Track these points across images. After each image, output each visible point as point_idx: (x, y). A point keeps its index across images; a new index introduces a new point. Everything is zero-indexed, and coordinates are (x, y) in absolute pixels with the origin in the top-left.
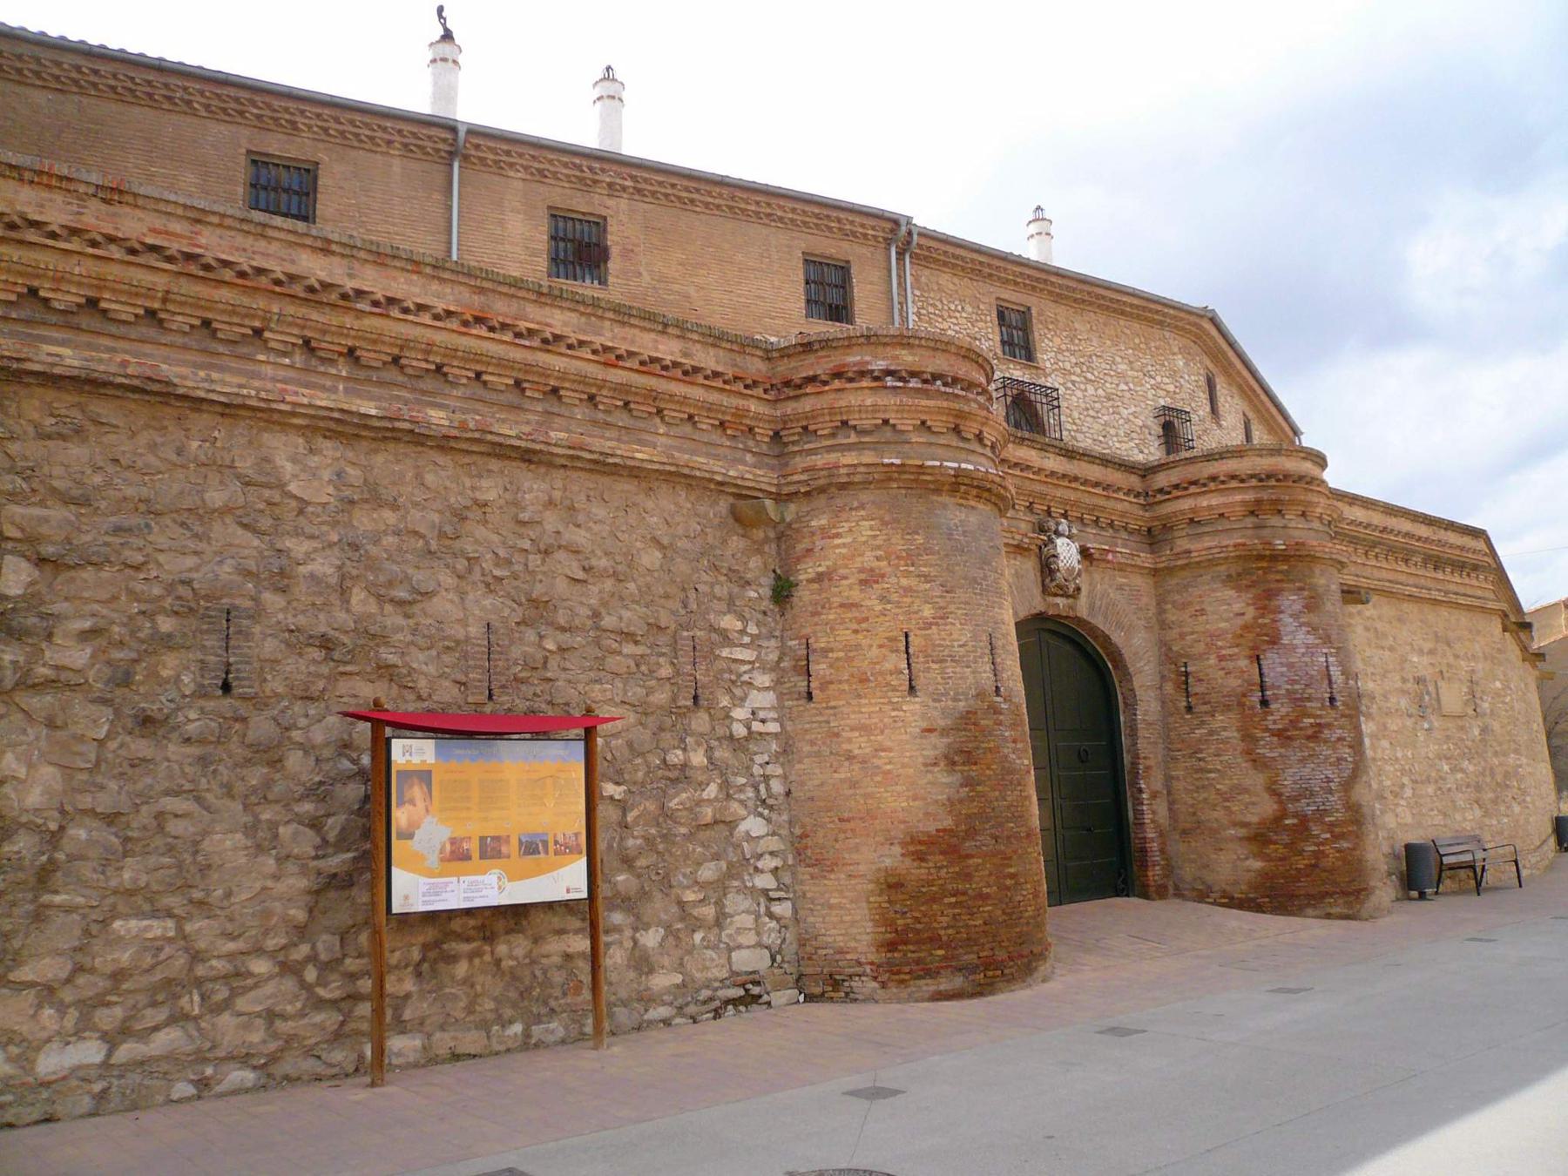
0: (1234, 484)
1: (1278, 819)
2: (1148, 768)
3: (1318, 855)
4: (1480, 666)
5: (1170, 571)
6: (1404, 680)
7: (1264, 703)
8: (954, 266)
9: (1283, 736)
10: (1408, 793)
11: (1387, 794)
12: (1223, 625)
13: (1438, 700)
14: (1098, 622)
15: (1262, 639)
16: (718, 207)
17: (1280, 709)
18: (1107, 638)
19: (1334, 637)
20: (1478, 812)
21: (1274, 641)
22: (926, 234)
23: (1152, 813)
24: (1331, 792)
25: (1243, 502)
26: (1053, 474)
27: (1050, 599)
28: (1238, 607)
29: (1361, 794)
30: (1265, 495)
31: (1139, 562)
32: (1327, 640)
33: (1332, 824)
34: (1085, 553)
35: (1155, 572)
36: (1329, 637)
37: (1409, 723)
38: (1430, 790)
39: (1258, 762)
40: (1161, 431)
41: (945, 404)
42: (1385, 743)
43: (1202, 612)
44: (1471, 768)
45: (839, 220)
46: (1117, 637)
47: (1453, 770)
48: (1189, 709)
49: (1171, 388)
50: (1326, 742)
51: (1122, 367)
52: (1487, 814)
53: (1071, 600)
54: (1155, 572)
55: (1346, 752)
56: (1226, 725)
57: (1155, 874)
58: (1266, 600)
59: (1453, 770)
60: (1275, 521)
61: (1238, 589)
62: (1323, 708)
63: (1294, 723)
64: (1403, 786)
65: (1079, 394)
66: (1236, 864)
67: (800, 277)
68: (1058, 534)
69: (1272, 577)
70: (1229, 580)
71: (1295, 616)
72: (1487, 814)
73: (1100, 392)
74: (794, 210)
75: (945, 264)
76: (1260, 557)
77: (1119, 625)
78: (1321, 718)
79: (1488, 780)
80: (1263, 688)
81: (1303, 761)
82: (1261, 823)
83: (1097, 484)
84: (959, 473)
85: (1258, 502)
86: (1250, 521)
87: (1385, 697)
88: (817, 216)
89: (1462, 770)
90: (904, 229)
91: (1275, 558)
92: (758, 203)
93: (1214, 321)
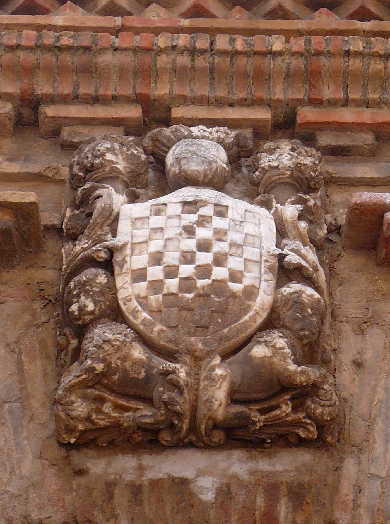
68: (155, 178)
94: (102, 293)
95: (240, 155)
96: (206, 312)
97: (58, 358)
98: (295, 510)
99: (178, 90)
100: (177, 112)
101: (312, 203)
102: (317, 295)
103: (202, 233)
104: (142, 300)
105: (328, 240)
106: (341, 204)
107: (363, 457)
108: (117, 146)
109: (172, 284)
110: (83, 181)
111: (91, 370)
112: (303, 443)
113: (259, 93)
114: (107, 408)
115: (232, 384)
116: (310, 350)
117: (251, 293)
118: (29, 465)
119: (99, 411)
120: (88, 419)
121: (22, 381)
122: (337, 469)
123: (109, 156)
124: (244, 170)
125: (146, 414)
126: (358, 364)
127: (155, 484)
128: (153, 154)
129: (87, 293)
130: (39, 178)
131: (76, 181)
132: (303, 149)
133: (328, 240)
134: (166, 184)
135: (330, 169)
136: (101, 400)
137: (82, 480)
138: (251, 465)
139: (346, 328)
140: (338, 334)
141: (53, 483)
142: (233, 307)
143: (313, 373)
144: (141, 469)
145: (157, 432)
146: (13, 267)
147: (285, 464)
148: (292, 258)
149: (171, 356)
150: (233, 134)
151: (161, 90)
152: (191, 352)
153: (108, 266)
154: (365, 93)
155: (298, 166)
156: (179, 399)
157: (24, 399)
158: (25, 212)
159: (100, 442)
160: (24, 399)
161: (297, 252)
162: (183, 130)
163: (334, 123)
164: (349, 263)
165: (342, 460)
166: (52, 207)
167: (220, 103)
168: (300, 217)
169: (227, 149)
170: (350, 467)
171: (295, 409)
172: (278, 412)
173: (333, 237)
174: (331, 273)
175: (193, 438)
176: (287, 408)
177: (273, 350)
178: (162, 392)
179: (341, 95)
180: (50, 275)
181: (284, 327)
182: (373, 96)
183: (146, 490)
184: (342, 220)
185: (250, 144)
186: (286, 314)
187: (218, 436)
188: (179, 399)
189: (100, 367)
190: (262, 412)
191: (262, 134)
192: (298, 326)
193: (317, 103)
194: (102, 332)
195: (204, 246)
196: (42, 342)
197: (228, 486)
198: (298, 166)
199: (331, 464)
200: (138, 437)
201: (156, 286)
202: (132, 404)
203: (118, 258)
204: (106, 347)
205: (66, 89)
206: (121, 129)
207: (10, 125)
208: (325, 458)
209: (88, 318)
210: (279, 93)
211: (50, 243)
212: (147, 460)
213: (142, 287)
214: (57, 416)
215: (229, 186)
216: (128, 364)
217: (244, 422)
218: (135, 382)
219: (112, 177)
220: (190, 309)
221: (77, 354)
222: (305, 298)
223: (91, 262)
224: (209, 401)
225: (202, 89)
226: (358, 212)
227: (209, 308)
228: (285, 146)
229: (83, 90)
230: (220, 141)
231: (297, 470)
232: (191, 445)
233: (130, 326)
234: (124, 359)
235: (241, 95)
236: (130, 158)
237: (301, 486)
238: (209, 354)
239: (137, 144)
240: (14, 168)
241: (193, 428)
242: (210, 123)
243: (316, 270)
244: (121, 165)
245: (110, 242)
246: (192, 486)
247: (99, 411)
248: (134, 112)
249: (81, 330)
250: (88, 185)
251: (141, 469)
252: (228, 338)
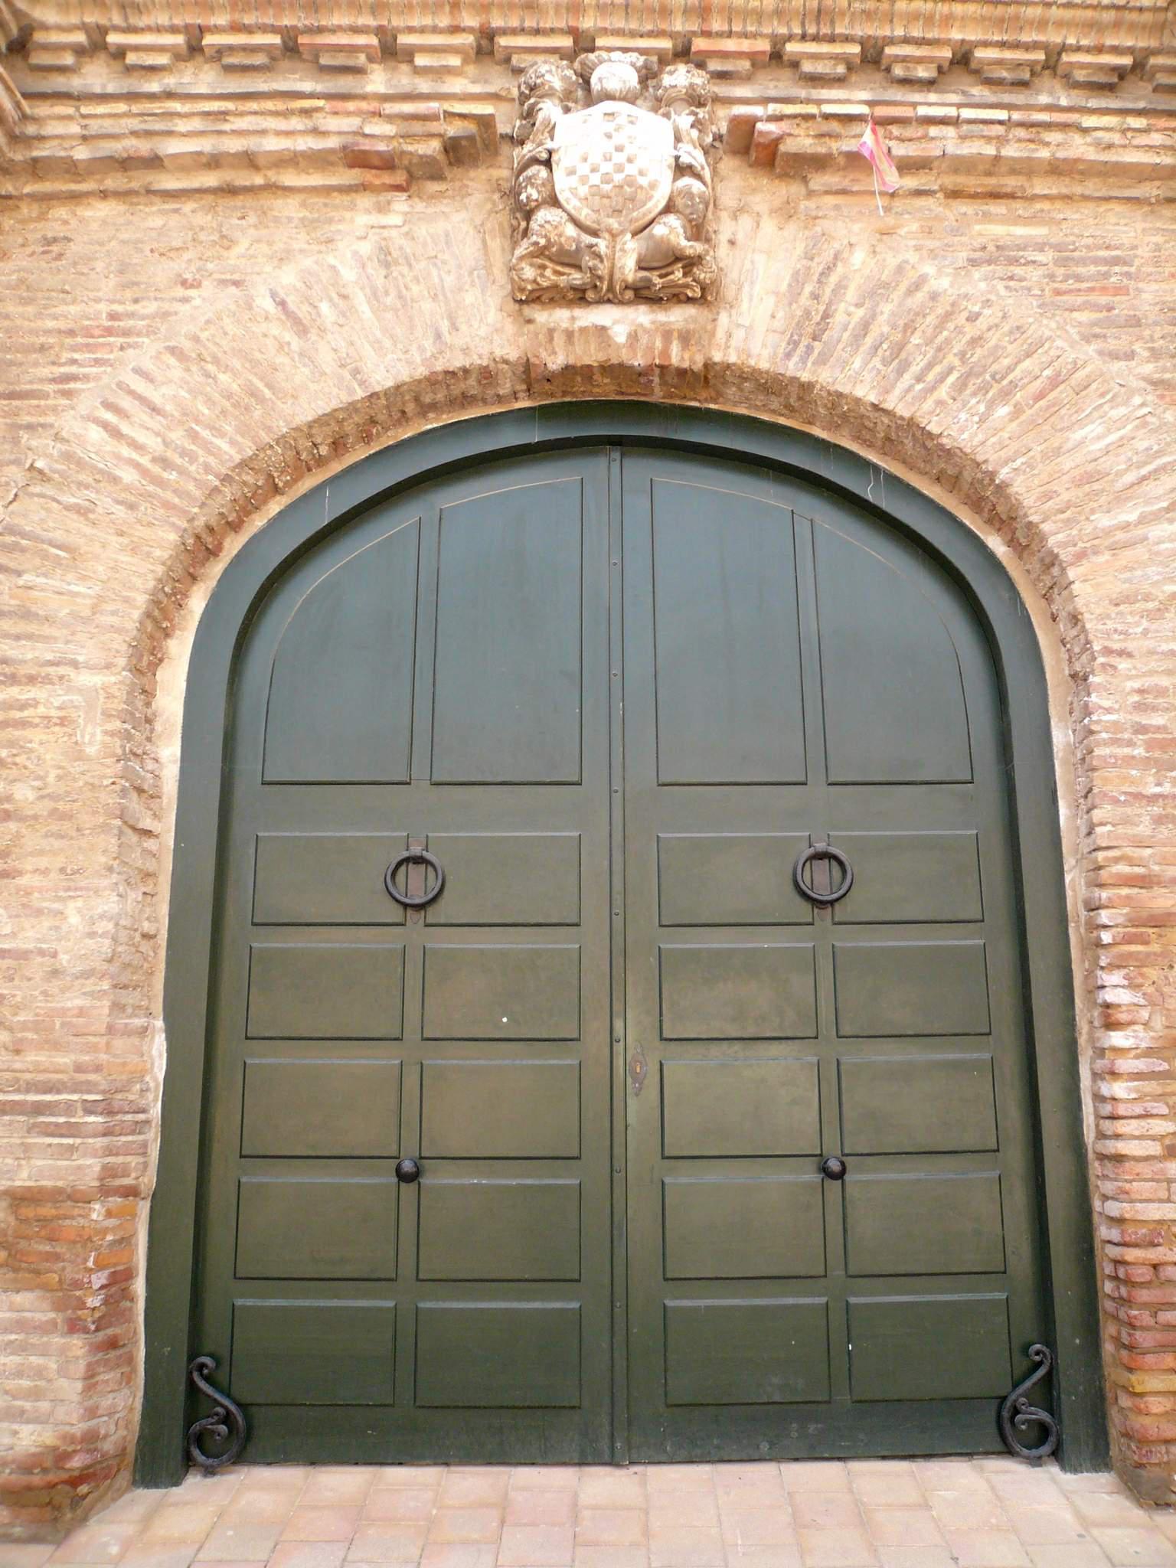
14: (855, 377)
31: (1079, 148)
46: (964, 426)
68: (584, 92)
77: (981, 379)
94: (543, 185)
95: (648, 76)
96: (620, 199)
97: (512, 236)
98: (683, 349)
99: (601, 24)
100: (600, 42)
101: (701, 116)
102: (703, 188)
103: (618, 139)
104: (573, 191)
105: (713, 146)
106: (722, 120)
107: (733, 312)
108: (554, 68)
109: (595, 179)
110: (528, 97)
111: (536, 243)
112: (690, 300)
113: (664, 26)
114: (548, 272)
115: (640, 255)
116: (697, 230)
117: (653, 186)
118: (493, 316)
119: (542, 275)
120: (535, 281)
121: (486, 254)
122: (714, 320)
123: (548, 77)
124: (651, 90)
125: (576, 278)
126: (732, 243)
127: (583, 330)
128: (582, 76)
129: (532, 185)
130: (495, 97)
131: (523, 98)
132: (696, 71)
133: (713, 146)
134: (591, 98)
135: (716, 89)
136: (543, 267)
137: (531, 327)
138: (652, 317)
139: (724, 215)
140: (718, 219)
141: (510, 328)
142: (641, 196)
143: (698, 247)
144: (573, 319)
145: (584, 291)
146: (477, 167)
147: (677, 316)
148: (685, 159)
149: (595, 233)
150: (642, 59)
151: (587, 23)
152: (610, 231)
153: (548, 163)
154: (744, 26)
155: (692, 85)
156: (600, 265)
157: (488, 267)
158: (485, 123)
159: (543, 299)
160: (488, 267)
161: (689, 154)
162: (604, 55)
163: (720, 51)
164: (728, 164)
165: (718, 313)
166: (507, 122)
167: (633, 34)
168: (692, 126)
169: (638, 71)
170: (723, 319)
171: (685, 275)
172: (671, 277)
173: (717, 144)
174: (715, 172)
175: (611, 296)
176: (679, 274)
177: (671, 230)
178: (588, 261)
179: (726, 28)
180: (505, 173)
181: (678, 211)
182: (751, 28)
183: (576, 334)
184: (724, 130)
185: (655, 67)
186: (680, 202)
187: (629, 294)
188: (600, 265)
189: (543, 242)
190: (661, 276)
191: (665, 60)
192: (688, 211)
193: (707, 34)
194: (543, 215)
195: (619, 149)
196: (500, 224)
197: (635, 332)
198: (692, 85)
199: (710, 317)
200: (571, 295)
201: (584, 180)
202: (566, 270)
203: (555, 158)
204: (547, 226)
205: (514, 23)
206: (557, 56)
207: (472, 53)
208: (706, 312)
209: (533, 204)
210: (679, 25)
211: (505, 148)
212: (578, 312)
213: (574, 181)
214: (512, 279)
215: (639, 102)
216: (563, 240)
217: (648, 285)
218: (568, 253)
219: (550, 94)
220: (609, 197)
221: (526, 233)
222: (695, 190)
223: (535, 161)
224: (622, 267)
225: (619, 23)
226: (736, 122)
227: (625, 196)
228: (682, 68)
229: (527, 24)
230: (633, 65)
231: (686, 320)
232: (609, 301)
233: (564, 210)
234: (560, 236)
235: (649, 27)
236: (565, 78)
237: (688, 332)
238: (622, 232)
239: (571, 68)
240: (477, 89)
241: (611, 288)
242: (625, 50)
243: (703, 168)
244: (558, 84)
245: (549, 145)
246: (609, 332)
247: (542, 275)
248: (566, 42)
249: (528, 215)
250: (532, 100)
251: (573, 319)
252: (637, 220)
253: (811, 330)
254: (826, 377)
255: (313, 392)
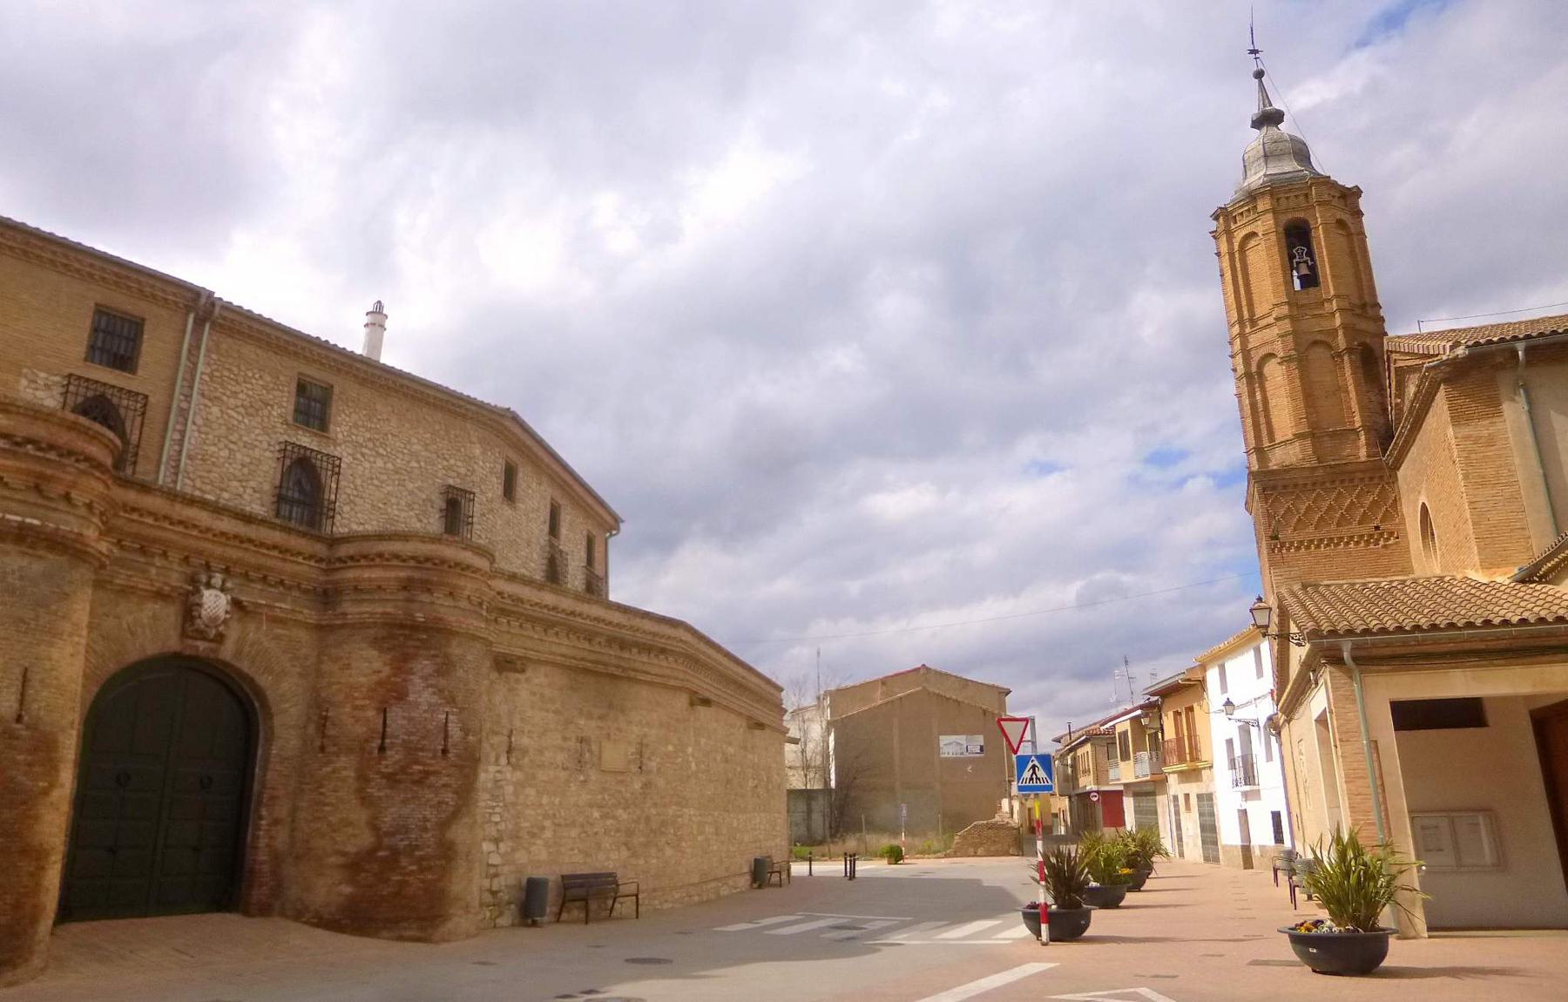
0: (395, 562)
1: (371, 853)
2: (273, 798)
3: (403, 884)
4: (654, 732)
5: (331, 628)
6: (565, 739)
7: (382, 749)
8: (259, 340)
9: (392, 779)
10: (548, 834)
11: (523, 834)
12: (362, 679)
13: (600, 758)
14: (245, 666)
15: (391, 694)
16: (11, 248)
17: (394, 756)
18: (252, 681)
19: (459, 698)
20: (625, 853)
21: (401, 696)
22: (228, 307)
23: (269, 835)
24: (425, 830)
25: (398, 579)
26: (223, 534)
27: (190, 642)
28: (377, 665)
29: (459, 833)
30: (417, 575)
31: (300, 617)
32: (451, 701)
33: (422, 858)
34: (236, 604)
35: (319, 628)
36: (454, 700)
37: (563, 775)
38: (574, 833)
39: (365, 800)
40: (444, 506)
41: (23, 466)
42: (531, 792)
43: (348, 666)
44: (625, 816)
45: (139, 282)
46: (264, 681)
47: (604, 817)
48: (322, 749)
49: (463, 471)
50: (430, 787)
51: (416, 447)
52: (635, 855)
53: (213, 645)
54: (319, 628)
55: (449, 797)
56: (346, 766)
57: (258, 894)
58: (402, 662)
59: (604, 817)
60: (425, 597)
61: (381, 650)
62: (434, 757)
63: (404, 770)
64: (543, 828)
65: (367, 465)
66: (329, 888)
67: (87, 323)
68: (209, 586)
69: (411, 643)
70: (375, 642)
71: (424, 678)
72: (635, 855)
73: (389, 466)
74: (92, 266)
75: (250, 337)
76: (402, 626)
78: (444, 767)
79: (641, 826)
80: (383, 737)
81: (405, 802)
82: (356, 854)
83: (275, 547)
84: (22, 526)
85: (410, 580)
86: (402, 595)
87: (541, 751)
88: (116, 274)
89: (614, 818)
90: (203, 300)
91: (415, 627)
92: (54, 253)
93: (515, 419)
253: (238, 653)
254: (238, 665)
255: (133, 656)
